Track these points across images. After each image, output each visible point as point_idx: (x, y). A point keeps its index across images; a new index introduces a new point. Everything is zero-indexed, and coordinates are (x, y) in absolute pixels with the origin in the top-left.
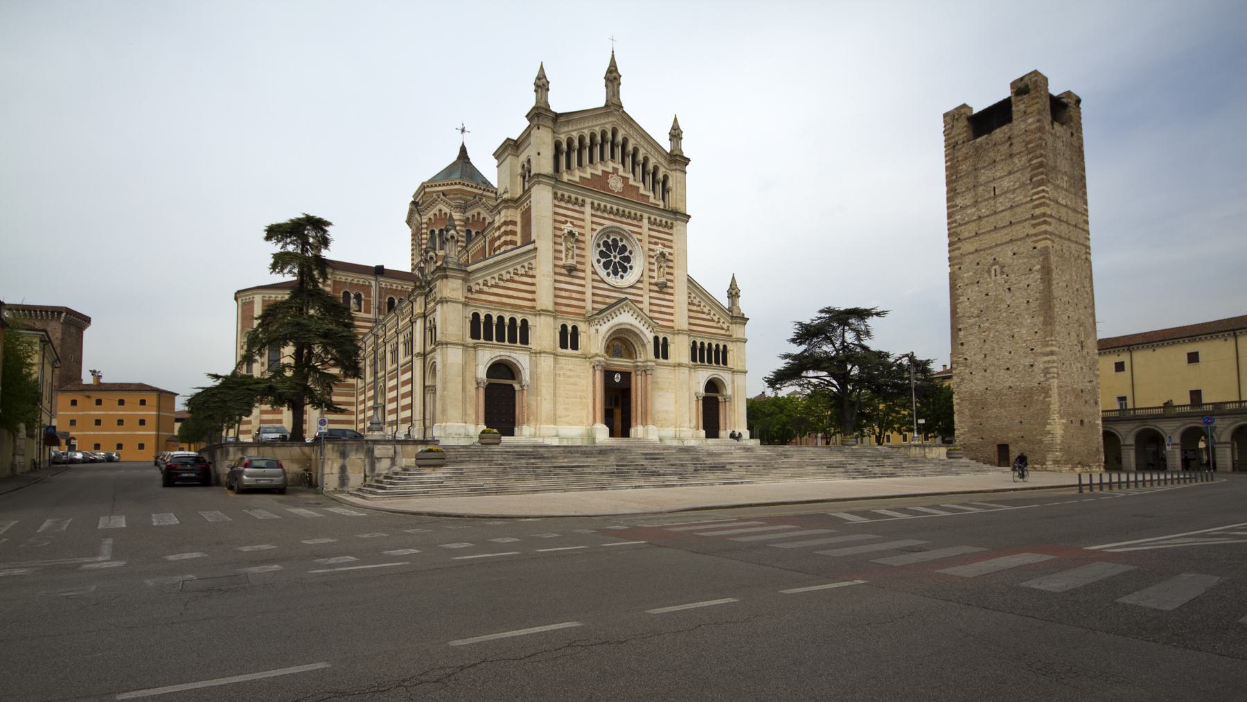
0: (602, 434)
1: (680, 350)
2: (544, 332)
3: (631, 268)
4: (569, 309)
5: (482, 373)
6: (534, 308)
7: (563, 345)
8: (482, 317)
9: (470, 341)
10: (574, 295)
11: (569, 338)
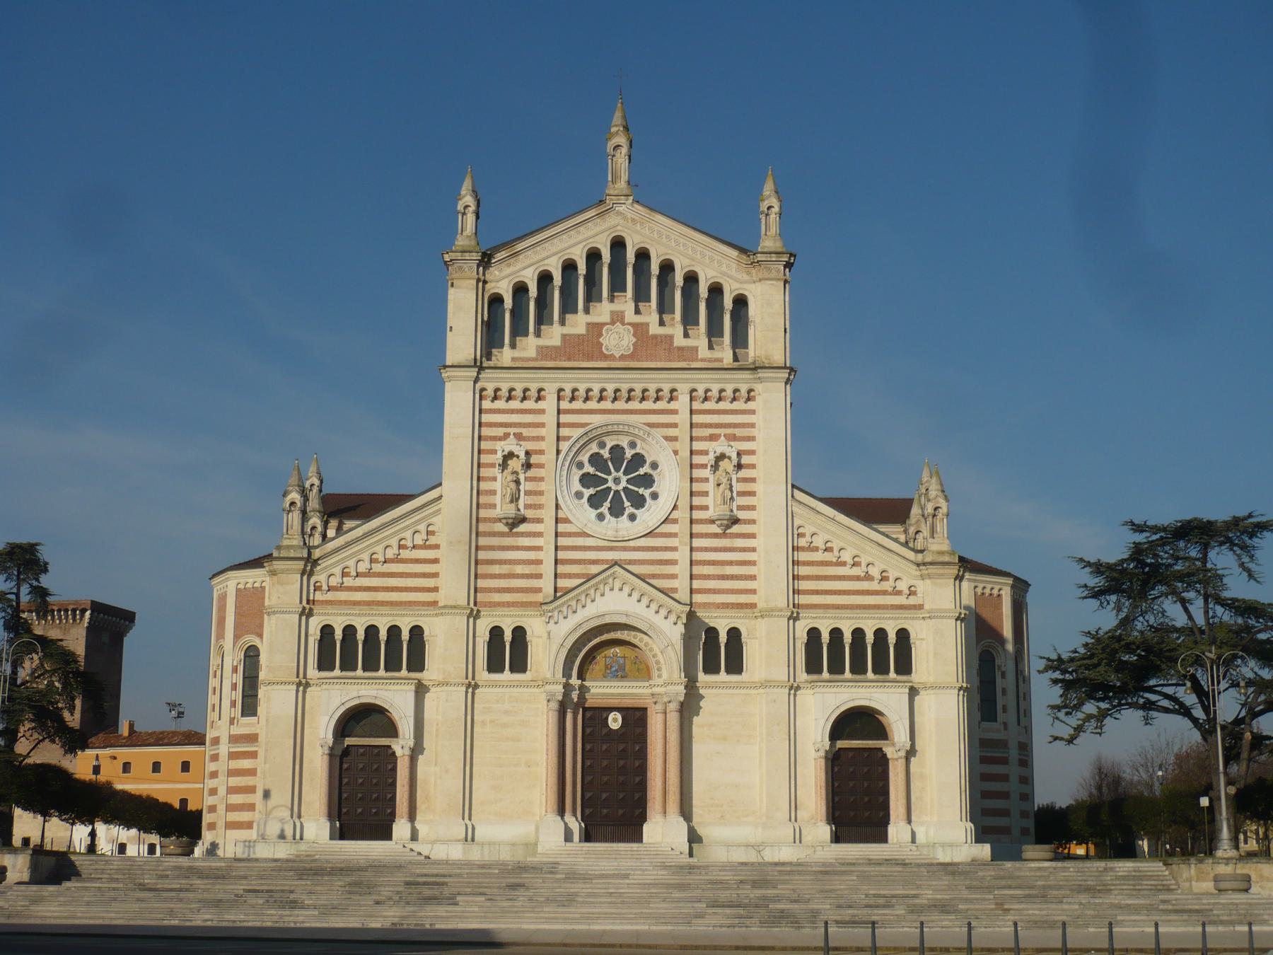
1: (769, 649)
2: (448, 645)
3: (655, 496)
4: (507, 597)
6: (435, 603)
7: (495, 665)
10: (519, 569)
11: (507, 652)
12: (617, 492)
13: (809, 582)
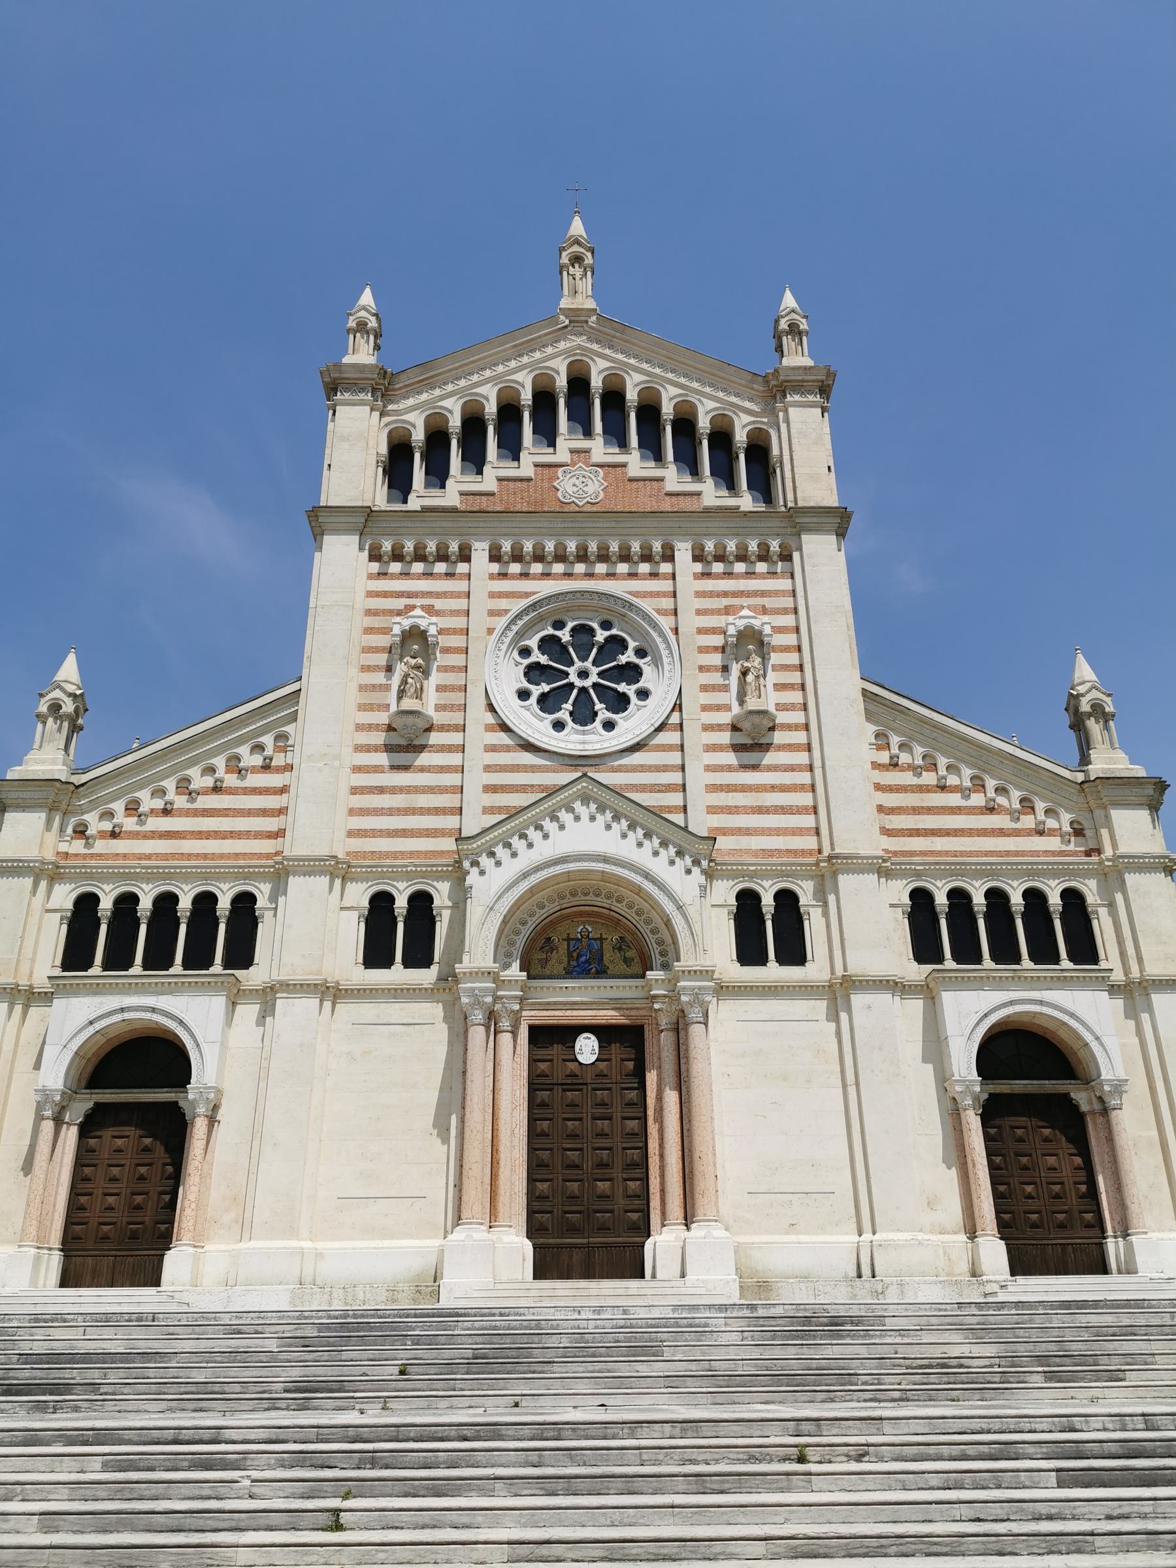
0: (492, 1264)
1: (864, 926)
2: (311, 930)
3: (523, 695)
5: (963, 1061)
8: (768, 901)
9: (917, 972)
12: (583, 690)
13: (903, 817)
